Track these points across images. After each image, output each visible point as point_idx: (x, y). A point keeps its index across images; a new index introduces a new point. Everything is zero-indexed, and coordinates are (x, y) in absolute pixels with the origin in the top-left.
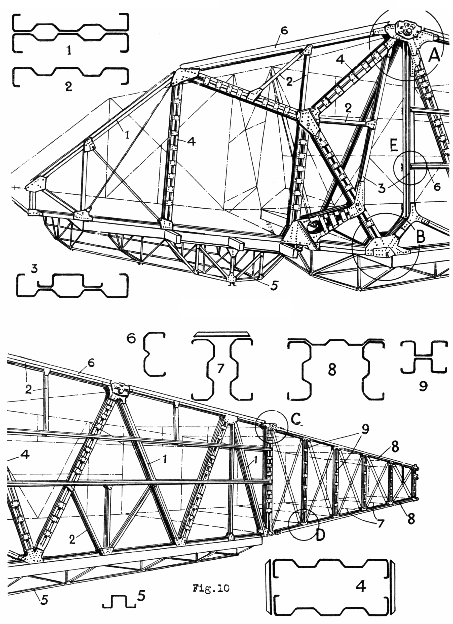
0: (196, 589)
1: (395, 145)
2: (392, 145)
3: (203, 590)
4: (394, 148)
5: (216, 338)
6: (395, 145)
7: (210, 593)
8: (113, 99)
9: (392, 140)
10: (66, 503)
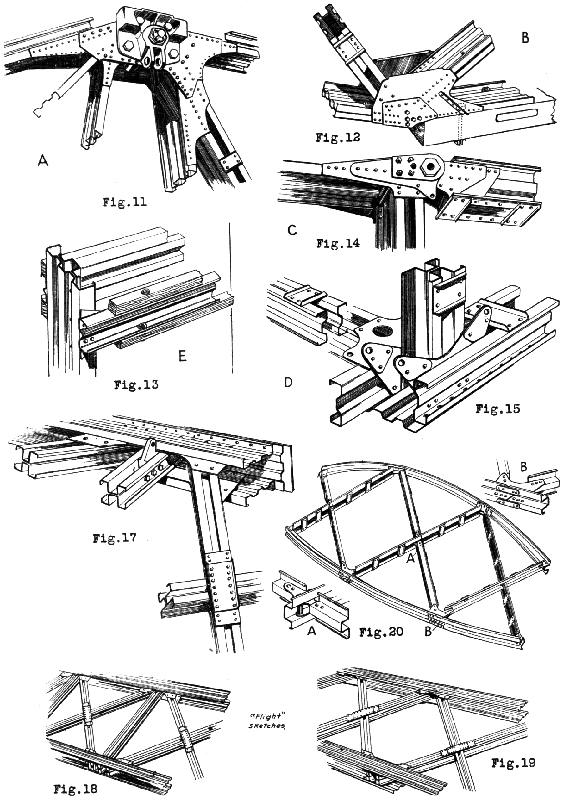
0: (320, 139)
1: (184, 356)
2: (180, 355)
3: (126, 387)
4: (182, 358)
5: (452, 409)
6: (184, 356)
7: (497, 414)
8: (422, 426)
9: (180, 351)
10: (157, 24)
